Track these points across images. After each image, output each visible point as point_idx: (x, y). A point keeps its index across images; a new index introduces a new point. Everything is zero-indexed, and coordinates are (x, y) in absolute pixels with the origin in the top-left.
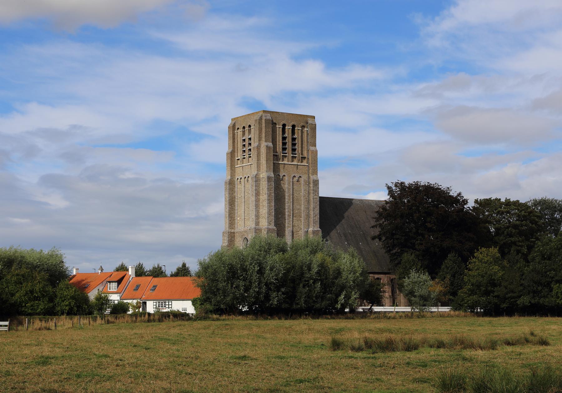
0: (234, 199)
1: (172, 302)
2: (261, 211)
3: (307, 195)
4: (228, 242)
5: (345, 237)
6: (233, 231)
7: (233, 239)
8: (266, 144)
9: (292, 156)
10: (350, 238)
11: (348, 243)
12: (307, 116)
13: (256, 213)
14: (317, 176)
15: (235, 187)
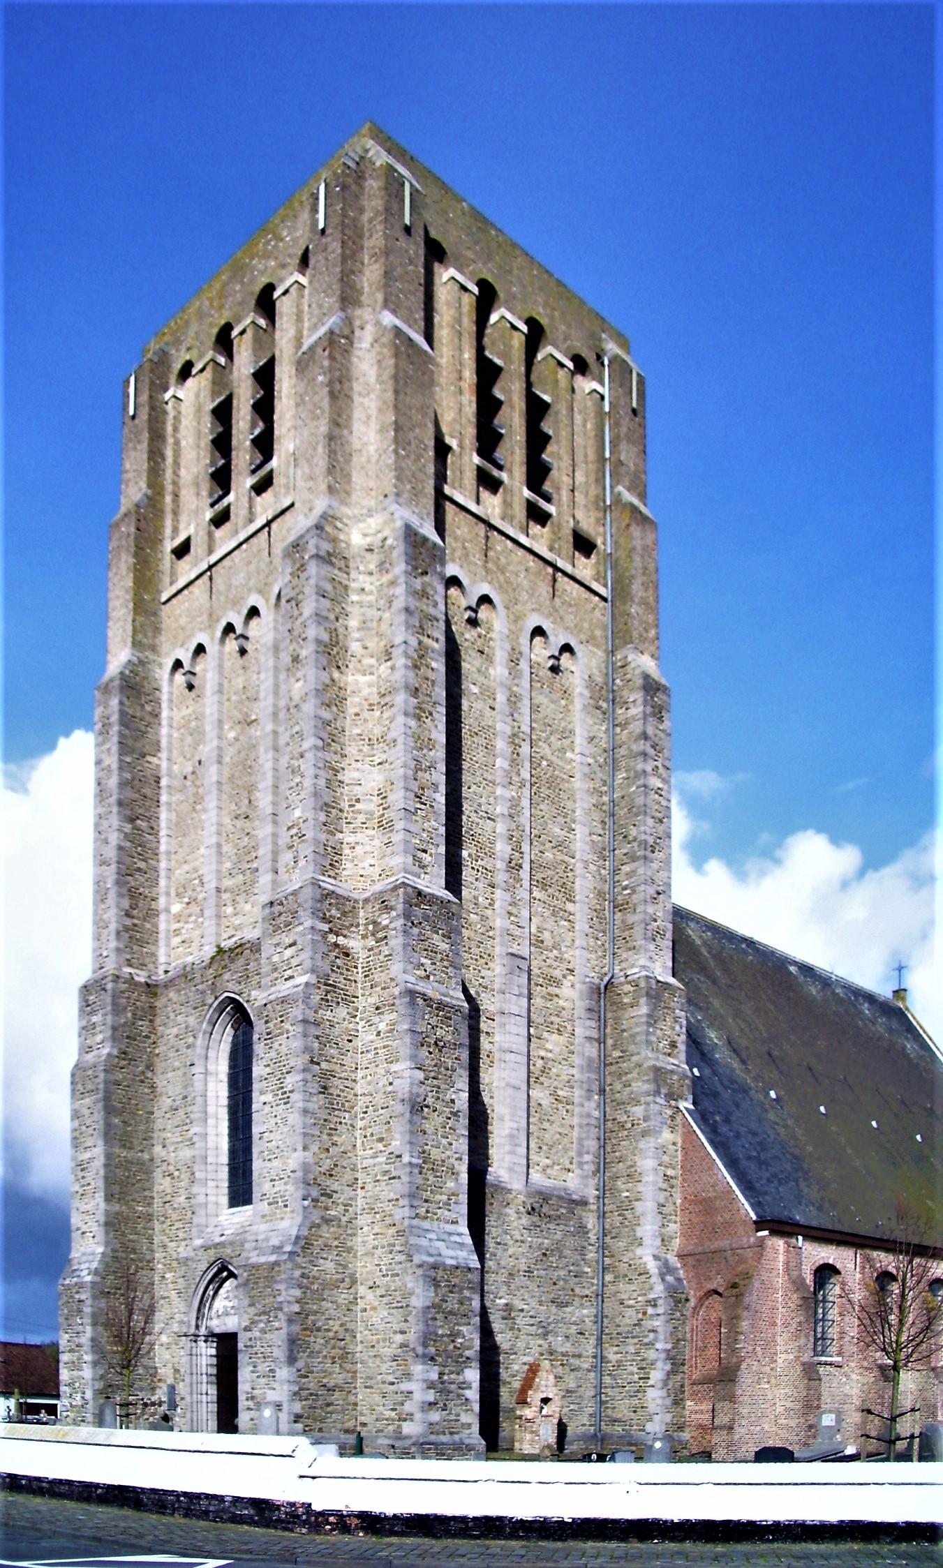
0: (147, 791)
2: (356, 775)
4: (114, 1039)
7: (143, 1026)
8: (388, 319)
13: (322, 782)
15: (156, 716)
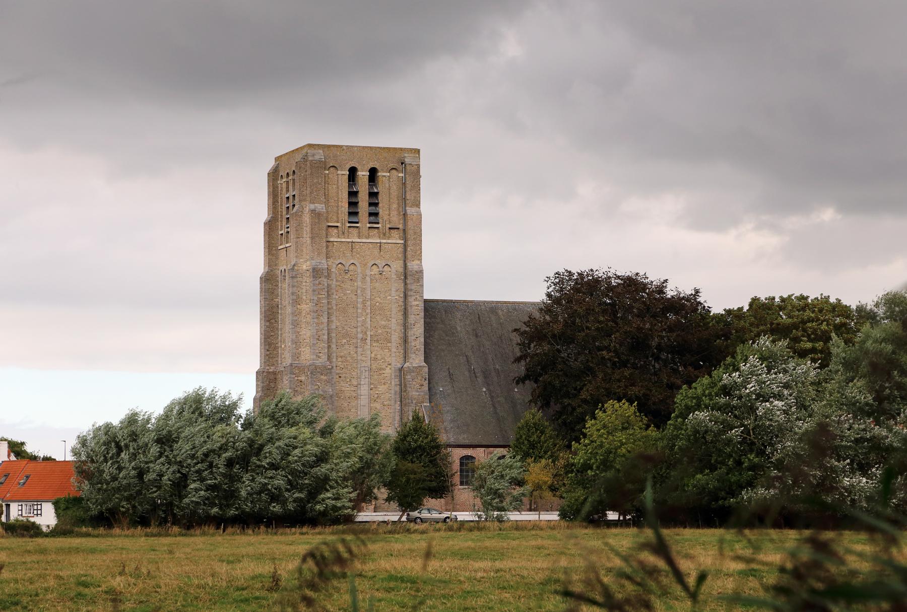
0: (275, 310)
1: (41, 504)
3: (402, 300)
4: (262, 391)
5: (485, 377)
6: (272, 369)
9: (369, 228)
10: (495, 379)
11: (488, 390)
12: (401, 149)
13: (294, 337)
14: (421, 262)
